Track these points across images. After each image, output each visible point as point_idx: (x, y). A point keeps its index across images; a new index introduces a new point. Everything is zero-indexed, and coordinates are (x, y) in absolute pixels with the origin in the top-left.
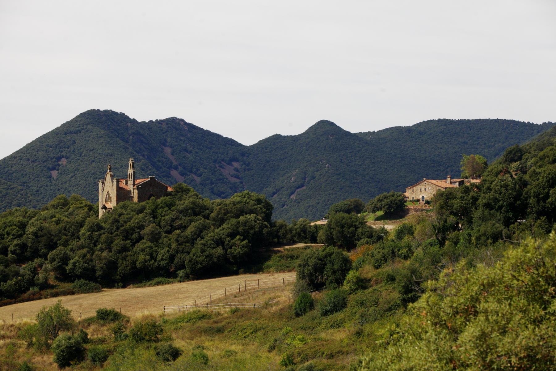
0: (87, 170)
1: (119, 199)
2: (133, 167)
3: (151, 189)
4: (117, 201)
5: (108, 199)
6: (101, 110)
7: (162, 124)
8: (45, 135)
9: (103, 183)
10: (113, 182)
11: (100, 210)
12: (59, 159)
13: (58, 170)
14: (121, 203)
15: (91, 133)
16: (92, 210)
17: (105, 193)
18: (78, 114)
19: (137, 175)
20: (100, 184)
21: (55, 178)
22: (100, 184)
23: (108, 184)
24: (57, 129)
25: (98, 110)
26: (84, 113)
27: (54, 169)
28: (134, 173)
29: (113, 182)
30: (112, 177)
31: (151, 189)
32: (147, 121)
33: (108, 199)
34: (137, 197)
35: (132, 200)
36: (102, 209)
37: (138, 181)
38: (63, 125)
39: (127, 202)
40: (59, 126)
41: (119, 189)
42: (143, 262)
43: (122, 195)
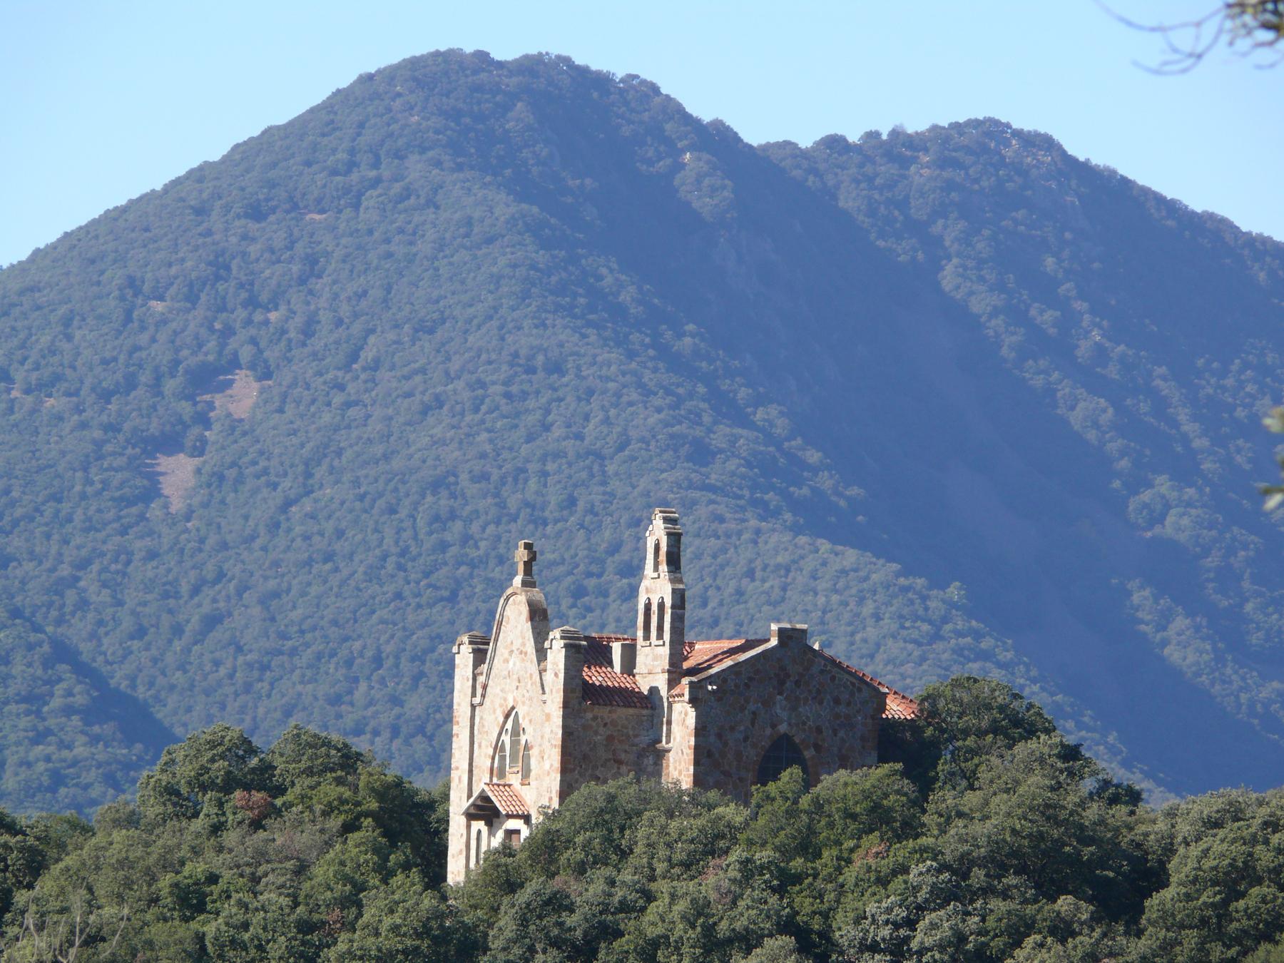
0: (386, 458)
1: (578, 759)
2: (674, 561)
3: (780, 707)
4: (564, 770)
5: (511, 753)
6: (499, 54)
7: (905, 163)
8: (122, 211)
9: (480, 656)
10: (541, 654)
11: (457, 823)
12: (209, 378)
13: (199, 449)
14: (592, 792)
15: (430, 214)
16: (411, 826)
17: (490, 719)
18: (345, 80)
19: (690, 612)
20: (464, 658)
21: (177, 506)
22: (464, 658)
23: (515, 663)
24: (200, 175)
25: (482, 56)
26: (390, 75)
27: (170, 443)
28: (680, 600)
29: (541, 654)
30: (539, 618)
31: (780, 707)
32: (805, 142)
33: (511, 753)
34: (689, 755)
35: (657, 771)
36: (470, 816)
37: (702, 650)
38: (244, 154)
39: (623, 787)
40: (216, 155)
41: (582, 698)
42: (950, 944)
43: (604, 725)
